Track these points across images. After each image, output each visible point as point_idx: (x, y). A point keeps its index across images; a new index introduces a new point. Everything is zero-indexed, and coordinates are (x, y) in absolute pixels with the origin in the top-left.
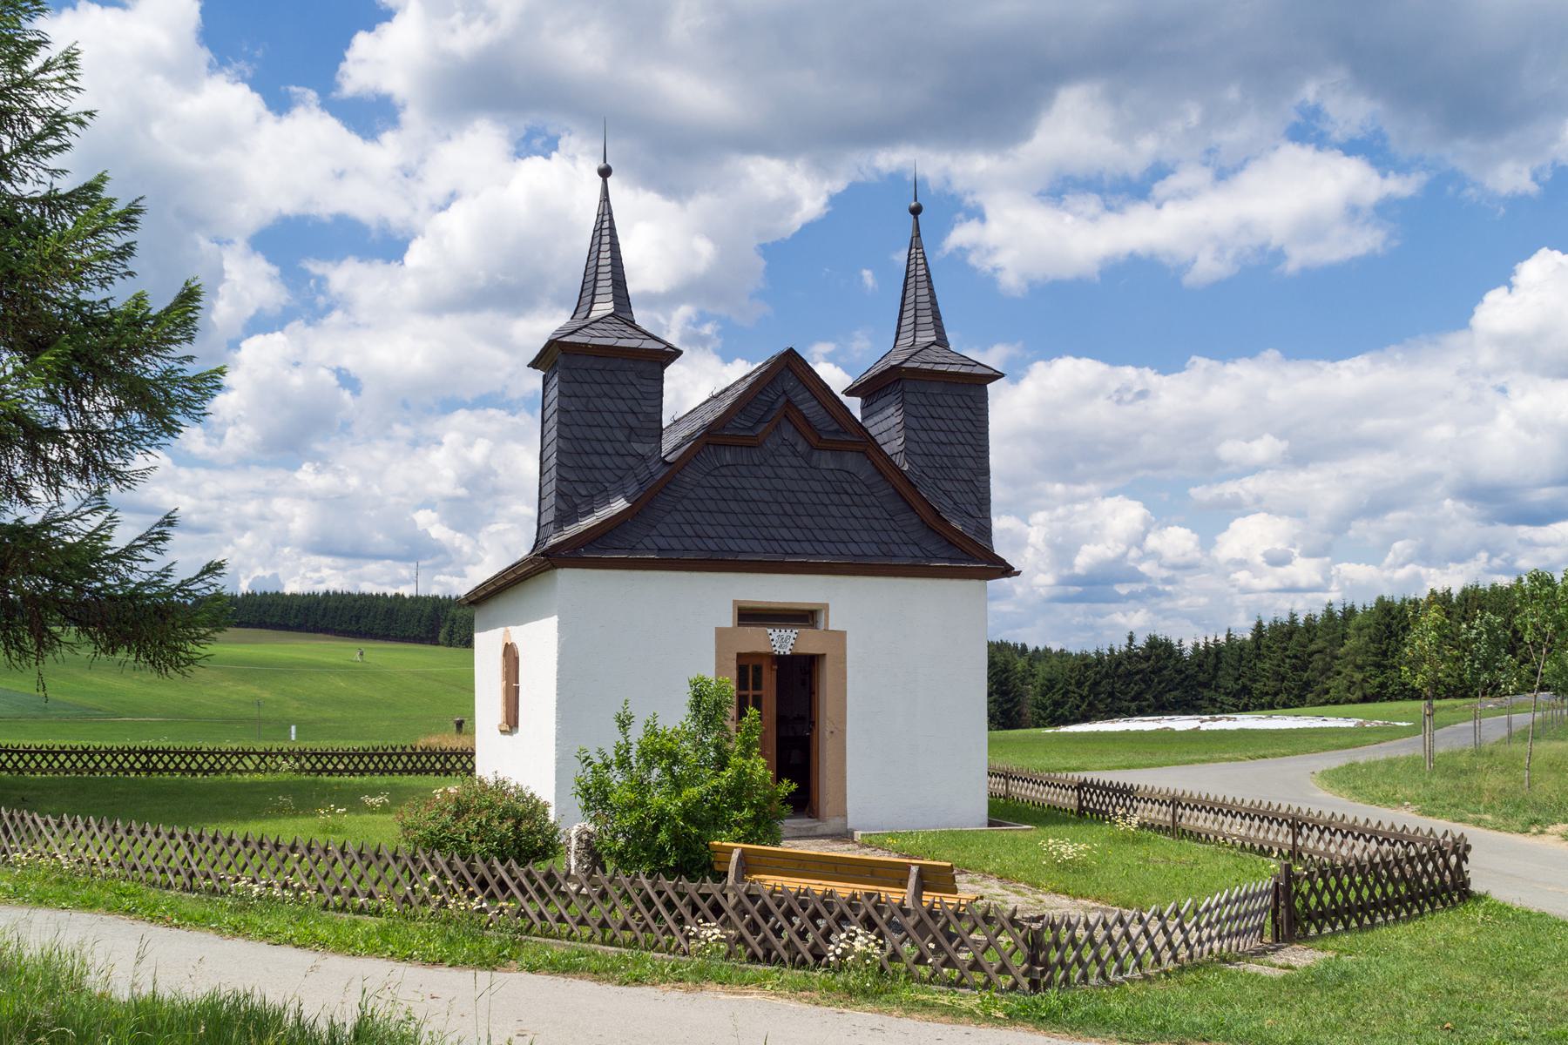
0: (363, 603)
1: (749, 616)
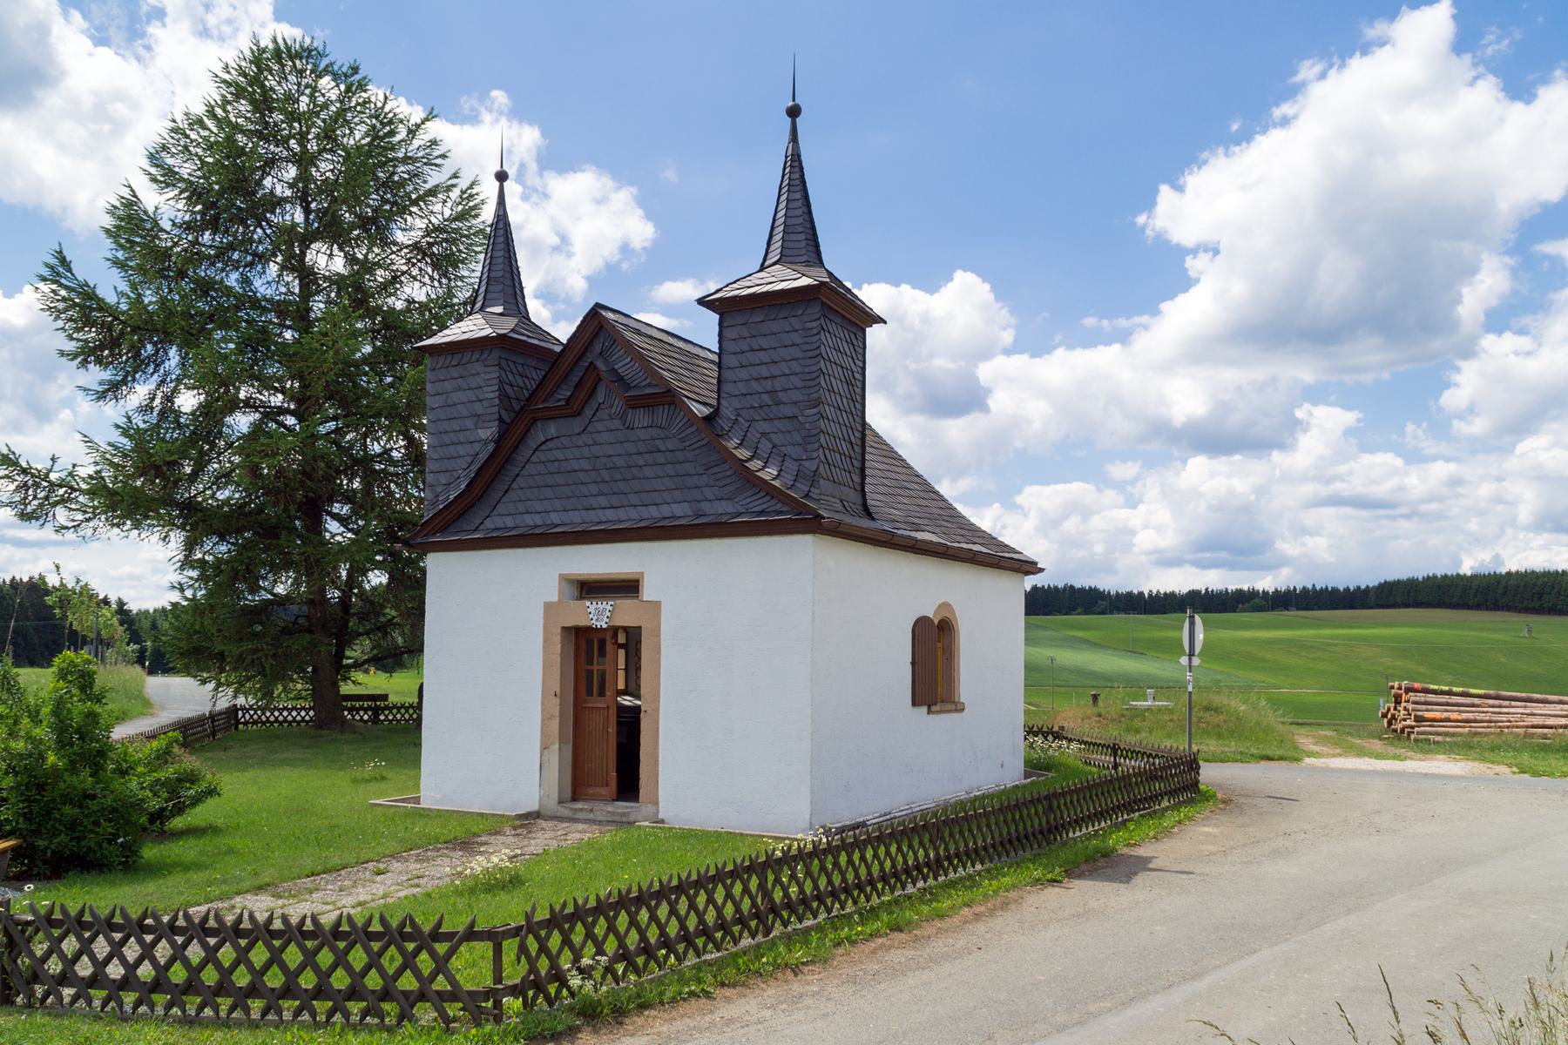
0: (1546, 580)
1: (589, 588)
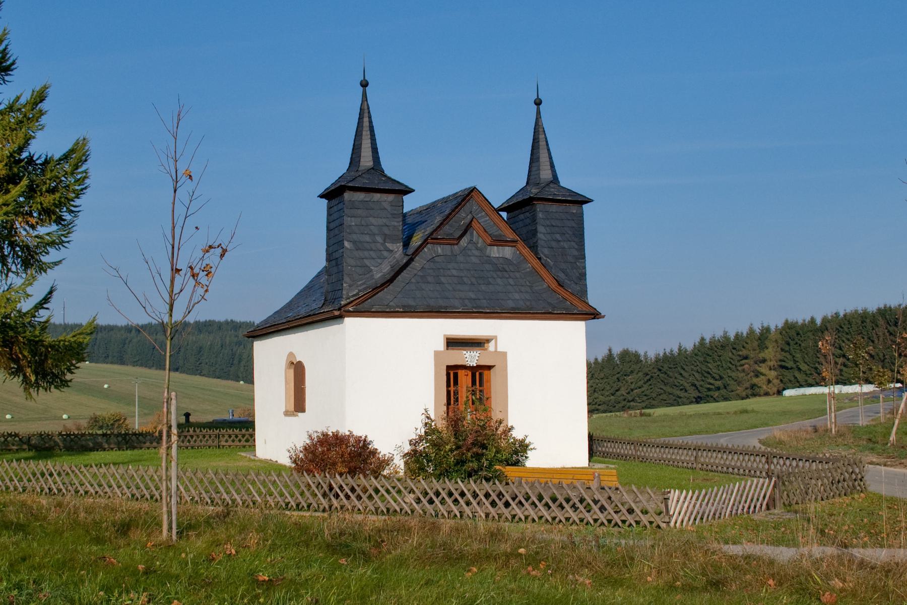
1: (453, 343)
